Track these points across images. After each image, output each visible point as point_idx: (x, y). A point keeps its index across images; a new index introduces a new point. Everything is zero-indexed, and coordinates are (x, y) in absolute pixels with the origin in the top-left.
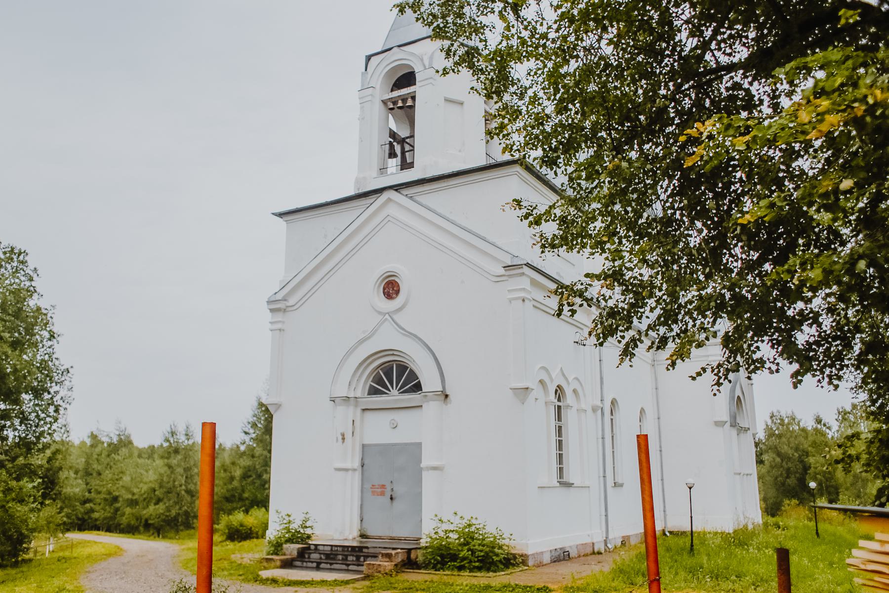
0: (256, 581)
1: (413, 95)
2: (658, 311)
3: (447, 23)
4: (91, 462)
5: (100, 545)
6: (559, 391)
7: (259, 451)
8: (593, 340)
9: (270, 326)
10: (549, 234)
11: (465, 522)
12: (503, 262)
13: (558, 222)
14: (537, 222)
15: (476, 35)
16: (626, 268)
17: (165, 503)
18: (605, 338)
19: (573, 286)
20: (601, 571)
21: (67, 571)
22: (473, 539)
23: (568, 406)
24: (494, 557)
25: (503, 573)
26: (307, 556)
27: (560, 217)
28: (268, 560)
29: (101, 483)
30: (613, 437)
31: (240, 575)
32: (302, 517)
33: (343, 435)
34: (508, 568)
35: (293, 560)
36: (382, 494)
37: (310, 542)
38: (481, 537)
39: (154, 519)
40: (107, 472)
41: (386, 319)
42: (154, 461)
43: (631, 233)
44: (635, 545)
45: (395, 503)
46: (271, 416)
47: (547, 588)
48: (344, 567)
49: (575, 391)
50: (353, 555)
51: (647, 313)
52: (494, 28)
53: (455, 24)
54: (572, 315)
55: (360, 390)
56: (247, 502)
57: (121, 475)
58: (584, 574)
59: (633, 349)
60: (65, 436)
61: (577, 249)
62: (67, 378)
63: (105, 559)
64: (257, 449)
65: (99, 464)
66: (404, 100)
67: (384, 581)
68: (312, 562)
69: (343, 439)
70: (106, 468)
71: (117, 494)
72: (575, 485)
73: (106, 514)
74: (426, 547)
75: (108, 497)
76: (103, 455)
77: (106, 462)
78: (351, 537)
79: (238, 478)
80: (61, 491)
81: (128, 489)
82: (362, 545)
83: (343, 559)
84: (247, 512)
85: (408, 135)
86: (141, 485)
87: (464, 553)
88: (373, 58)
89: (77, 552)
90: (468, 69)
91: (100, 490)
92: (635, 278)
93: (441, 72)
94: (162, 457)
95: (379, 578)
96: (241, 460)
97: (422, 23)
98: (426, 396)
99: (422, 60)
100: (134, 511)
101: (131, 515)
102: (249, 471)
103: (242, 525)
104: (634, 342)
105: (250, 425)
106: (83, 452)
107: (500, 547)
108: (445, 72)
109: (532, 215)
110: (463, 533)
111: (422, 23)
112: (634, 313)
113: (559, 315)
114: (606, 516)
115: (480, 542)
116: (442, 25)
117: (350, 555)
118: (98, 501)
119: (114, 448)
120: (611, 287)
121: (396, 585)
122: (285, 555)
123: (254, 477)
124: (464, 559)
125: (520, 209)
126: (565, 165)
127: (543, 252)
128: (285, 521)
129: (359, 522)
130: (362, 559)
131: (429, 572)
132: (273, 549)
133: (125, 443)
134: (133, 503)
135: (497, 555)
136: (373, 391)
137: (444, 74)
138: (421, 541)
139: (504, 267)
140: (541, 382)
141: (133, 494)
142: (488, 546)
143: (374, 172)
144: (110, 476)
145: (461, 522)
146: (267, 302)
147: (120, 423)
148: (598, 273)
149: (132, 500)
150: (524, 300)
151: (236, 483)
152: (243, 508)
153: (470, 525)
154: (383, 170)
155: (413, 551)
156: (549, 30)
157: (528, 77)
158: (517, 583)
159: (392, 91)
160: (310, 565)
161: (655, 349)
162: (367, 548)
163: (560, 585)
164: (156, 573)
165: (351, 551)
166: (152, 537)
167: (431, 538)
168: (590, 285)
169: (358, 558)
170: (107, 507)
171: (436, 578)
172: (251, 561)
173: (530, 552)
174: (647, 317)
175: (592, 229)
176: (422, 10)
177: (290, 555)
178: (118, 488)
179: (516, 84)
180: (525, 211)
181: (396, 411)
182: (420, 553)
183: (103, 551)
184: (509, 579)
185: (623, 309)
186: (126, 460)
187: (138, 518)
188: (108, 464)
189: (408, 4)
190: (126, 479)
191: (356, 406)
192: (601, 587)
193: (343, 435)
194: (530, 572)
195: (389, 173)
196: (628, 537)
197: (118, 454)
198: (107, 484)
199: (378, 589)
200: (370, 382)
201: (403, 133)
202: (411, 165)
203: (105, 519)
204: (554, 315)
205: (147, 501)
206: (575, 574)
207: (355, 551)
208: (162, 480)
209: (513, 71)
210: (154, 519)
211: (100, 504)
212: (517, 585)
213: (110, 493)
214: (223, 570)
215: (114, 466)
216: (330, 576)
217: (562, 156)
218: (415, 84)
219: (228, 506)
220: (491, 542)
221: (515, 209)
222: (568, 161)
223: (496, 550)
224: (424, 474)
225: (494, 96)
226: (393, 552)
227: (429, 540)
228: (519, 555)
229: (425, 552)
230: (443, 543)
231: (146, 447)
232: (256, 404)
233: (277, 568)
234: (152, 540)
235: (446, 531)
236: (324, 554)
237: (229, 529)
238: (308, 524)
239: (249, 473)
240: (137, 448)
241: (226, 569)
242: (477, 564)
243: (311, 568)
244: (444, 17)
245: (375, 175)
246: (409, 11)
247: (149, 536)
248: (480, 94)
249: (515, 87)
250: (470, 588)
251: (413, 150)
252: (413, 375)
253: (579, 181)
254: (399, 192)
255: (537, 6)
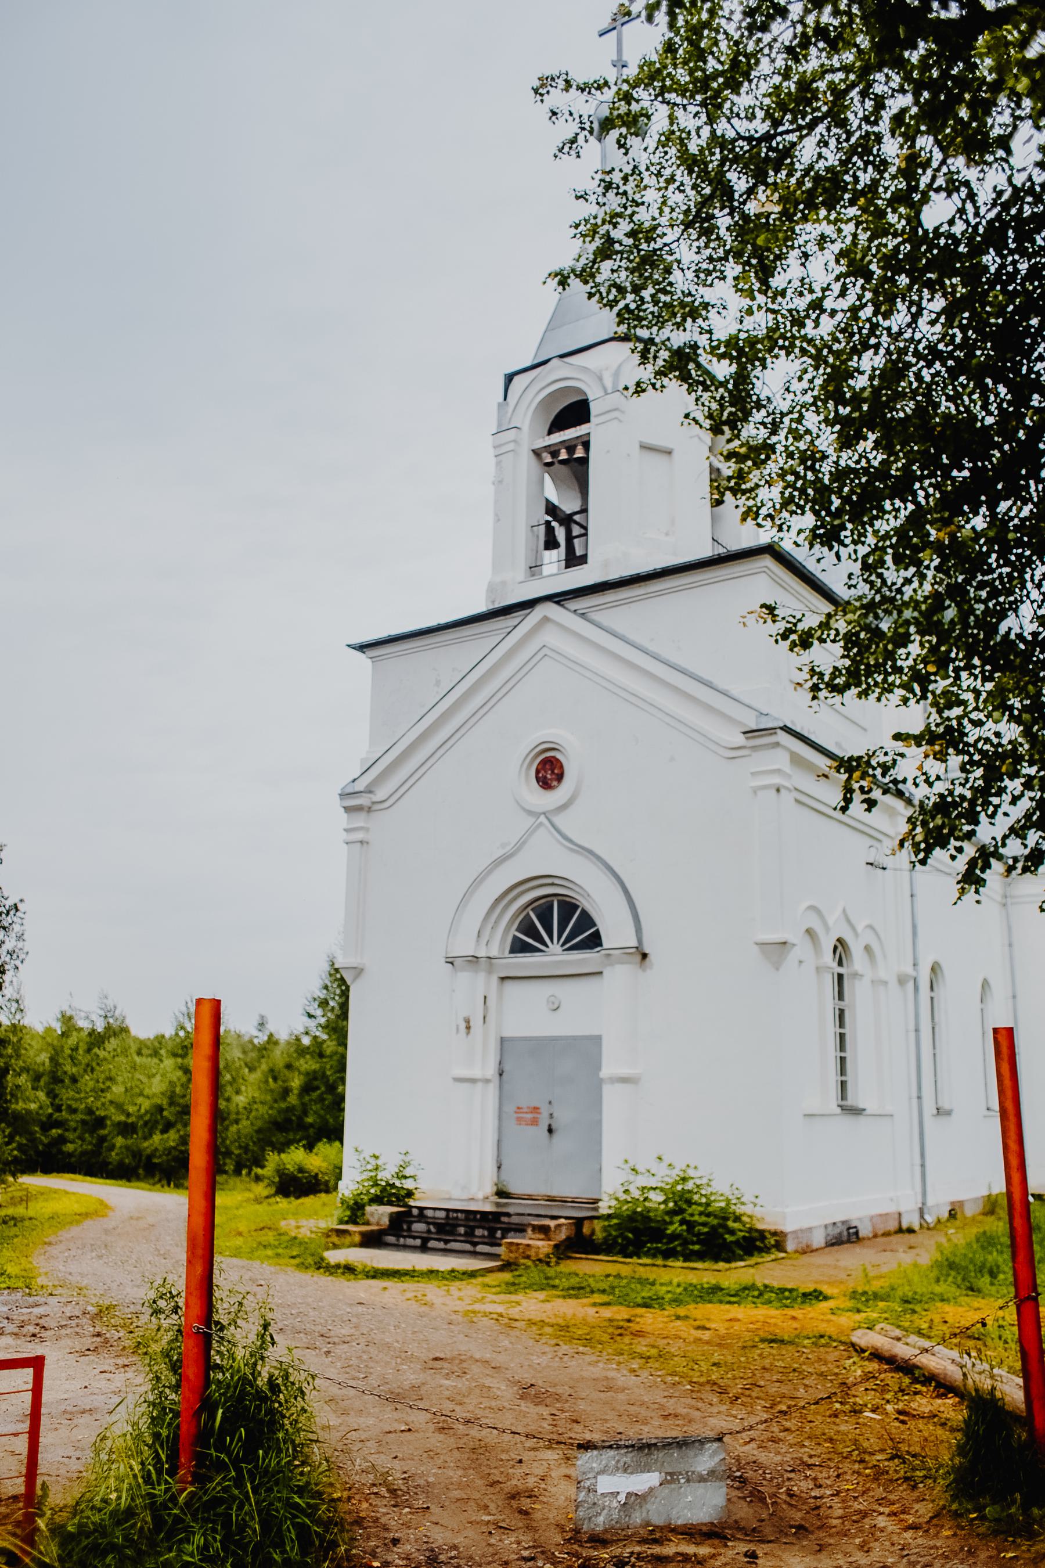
0: (319, 1268)
1: (586, 439)
2: (1025, 804)
3: (643, 303)
4: (61, 1061)
5: (73, 1198)
6: (840, 948)
7: (330, 1047)
8: (906, 854)
9: (344, 836)
10: (826, 667)
11: (675, 1174)
12: (740, 723)
13: (842, 643)
14: (805, 642)
15: (694, 321)
16: (971, 721)
17: (178, 1131)
18: (928, 851)
19: (870, 757)
20: (916, 1265)
21: (15, 1240)
22: (689, 1202)
23: (855, 975)
24: (727, 1236)
25: (742, 1264)
26: (405, 1227)
27: (845, 635)
28: (340, 1233)
29: (77, 1096)
30: (933, 1028)
31: (293, 1257)
32: (398, 1160)
33: (467, 1021)
34: (751, 1255)
35: (382, 1233)
36: (535, 1122)
37: (412, 1203)
38: (704, 1200)
39: (160, 1157)
40: (87, 1077)
41: (541, 824)
42: (161, 1061)
43: (976, 661)
44: (973, 1219)
45: (555, 1136)
46: (348, 988)
47: (821, 1293)
48: (468, 1247)
49: (867, 949)
50: (483, 1228)
51: (1005, 807)
52: (724, 308)
53: (656, 302)
54: (869, 810)
55: (497, 945)
56: (311, 1131)
57: (108, 1083)
58: (884, 1270)
59: (983, 871)
60: (18, 1017)
61: (876, 695)
62: (15, 919)
63: (78, 1222)
64: (329, 1043)
65: (75, 1065)
66: (571, 449)
67: (535, 1274)
68: (414, 1238)
69: (468, 1028)
70: (85, 1071)
71: (103, 1114)
72: (868, 1112)
73: (84, 1147)
74: (609, 1217)
75: (87, 1118)
76: (81, 1051)
77: (84, 1061)
78: (480, 1196)
79: (296, 1092)
80: (8, 1108)
81: (120, 1107)
82: (500, 1210)
83: (466, 1234)
84: (310, 1147)
85: (577, 508)
86: (140, 1100)
87: (675, 1227)
88: (516, 379)
89: (38, 1209)
90: (679, 383)
91: (74, 1105)
92: (987, 740)
93: (632, 390)
94: (175, 1055)
95: (527, 1267)
96: (302, 1061)
97: (599, 302)
98: (609, 955)
99: (600, 379)
100: (130, 1142)
101: (124, 1150)
102: (315, 1079)
103: (301, 1170)
104: (986, 856)
105: (317, 1003)
106: (49, 1044)
107: (737, 1219)
108: (639, 389)
109: (795, 632)
110: (673, 1193)
111: (599, 302)
112: (982, 805)
113: (844, 809)
114: (923, 1166)
115: (701, 1209)
116: (633, 306)
117: (479, 1227)
118: (73, 1124)
119: (97, 1040)
120: (941, 757)
121: (557, 1282)
122: (368, 1223)
123: (323, 1089)
124: (674, 1237)
125: (774, 621)
126: (855, 542)
127: (814, 698)
128: (370, 1167)
129: (496, 1169)
130: (499, 1234)
131: (614, 1258)
132: (348, 1213)
133: (116, 1031)
134: (126, 1129)
135: (732, 1232)
136: (519, 947)
137: (637, 392)
138: (600, 1204)
139: (745, 733)
140: (809, 932)
141: (128, 1115)
142: (716, 1217)
143: (520, 572)
144: (91, 1084)
145: (669, 1172)
146: (340, 795)
147: (106, 997)
148: (917, 732)
149: (126, 1124)
150: (778, 790)
151: (293, 1099)
152: (304, 1142)
153: (684, 1180)
154: (534, 568)
155: (586, 1224)
156: (827, 293)
157: (786, 395)
158: (767, 1282)
159: (550, 433)
160: (410, 1242)
161: (1019, 871)
162: (508, 1215)
163: (843, 1287)
164: (157, 1249)
165: (481, 1220)
166: (158, 1186)
167: (617, 1199)
168: (902, 755)
169: (492, 1232)
170: (87, 1135)
171: (625, 1270)
172: (312, 1232)
173: (788, 1228)
174: (1006, 814)
175: (904, 657)
176: (599, 279)
177: (378, 1224)
178: (103, 1104)
179: (765, 407)
180: (781, 626)
181: (565, 979)
182: (598, 1225)
183: (77, 1208)
184: (753, 1275)
185: (962, 797)
186: (116, 1059)
187: (137, 1154)
188: (88, 1065)
189: (573, 271)
190: (118, 1090)
191: (490, 971)
192: (915, 1293)
193: (467, 1021)
194: (788, 1262)
195: (545, 573)
196: (961, 1203)
197: (104, 1049)
198: (87, 1098)
199: (525, 1288)
200: (513, 932)
201: (569, 505)
202: (583, 560)
203: (84, 1153)
204: (835, 809)
205: (150, 1125)
206: (869, 1268)
207: (488, 1221)
208: (174, 1092)
209: (758, 384)
210: (160, 1157)
211: (75, 1130)
212: (766, 1286)
213: (90, 1111)
214: (265, 1247)
215: (98, 1068)
216: (444, 1263)
217: (849, 526)
218: (589, 421)
219: (279, 1137)
220: (722, 1209)
221: (765, 622)
222: (860, 535)
223: (730, 1224)
224: (607, 1090)
225: (726, 428)
226: (552, 1224)
227: (614, 1203)
228: (769, 1232)
229: (606, 1223)
230: (639, 1209)
231: (152, 1037)
232: (326, 967)
233: (355, 1246)
234: (159, 1190)
235: (644, 1188)
236: (434, 1224)
237: (280, 1177)
238: (408, 1172)
239: (316, 1083)
240: (136, 1039)
241: (270, 1245)
242: (697, 1247)
243: (413, 1248)
244: (636, 289)
245: (521, 578)
246: (574, 282)
247: (154, 1184)
248: (701, 427)
249: (763, 412)
250: (685, 1289)
251: (586, 535)
252: (587, 920)
253: (879, 571)
254: (562, 606)
255: (802, 268)
